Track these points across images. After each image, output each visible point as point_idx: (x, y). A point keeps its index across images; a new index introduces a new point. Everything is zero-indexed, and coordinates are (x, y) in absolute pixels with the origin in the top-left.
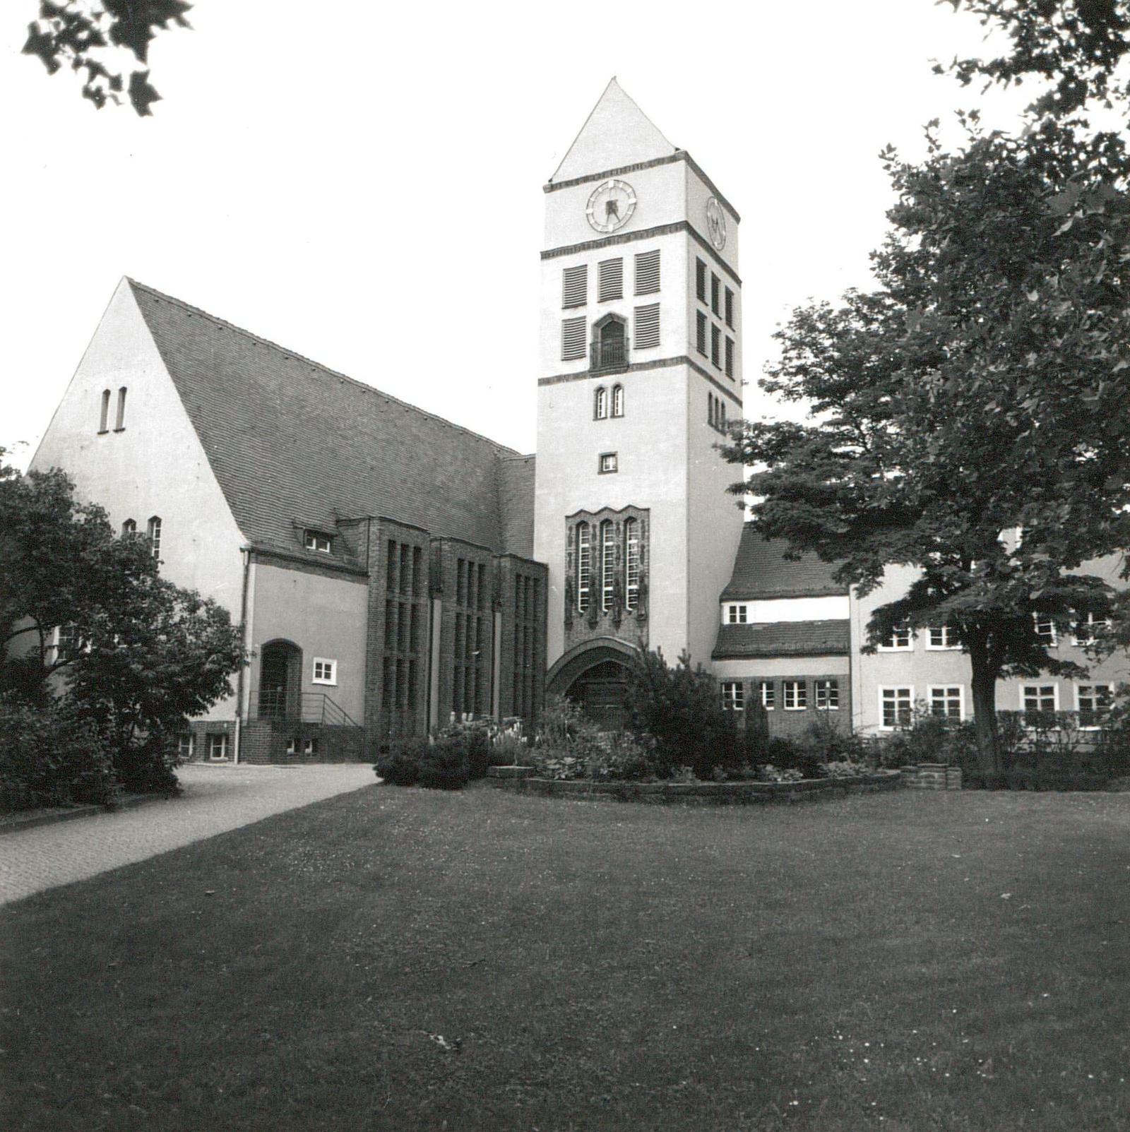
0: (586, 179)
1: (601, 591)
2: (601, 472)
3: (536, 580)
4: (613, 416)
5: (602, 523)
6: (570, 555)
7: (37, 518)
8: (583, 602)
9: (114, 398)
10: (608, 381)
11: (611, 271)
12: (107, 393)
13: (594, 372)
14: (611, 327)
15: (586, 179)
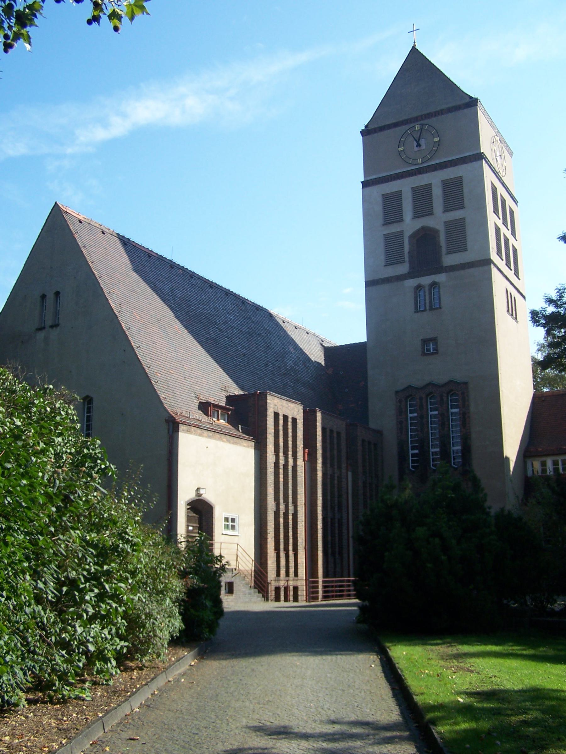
0: (396, 125)
1: (429, 451)
2: (424, 354)
3: (375, 445)
4: (431, 309)
5: (427, 395)
6: (401, 423)
7: (32, 20)
8: (413, 462)
10: (426, 281)
11: (422, 197)
12: (43, 297)
13: (411, 275)
14: (425, 239)
15: (396, 125)
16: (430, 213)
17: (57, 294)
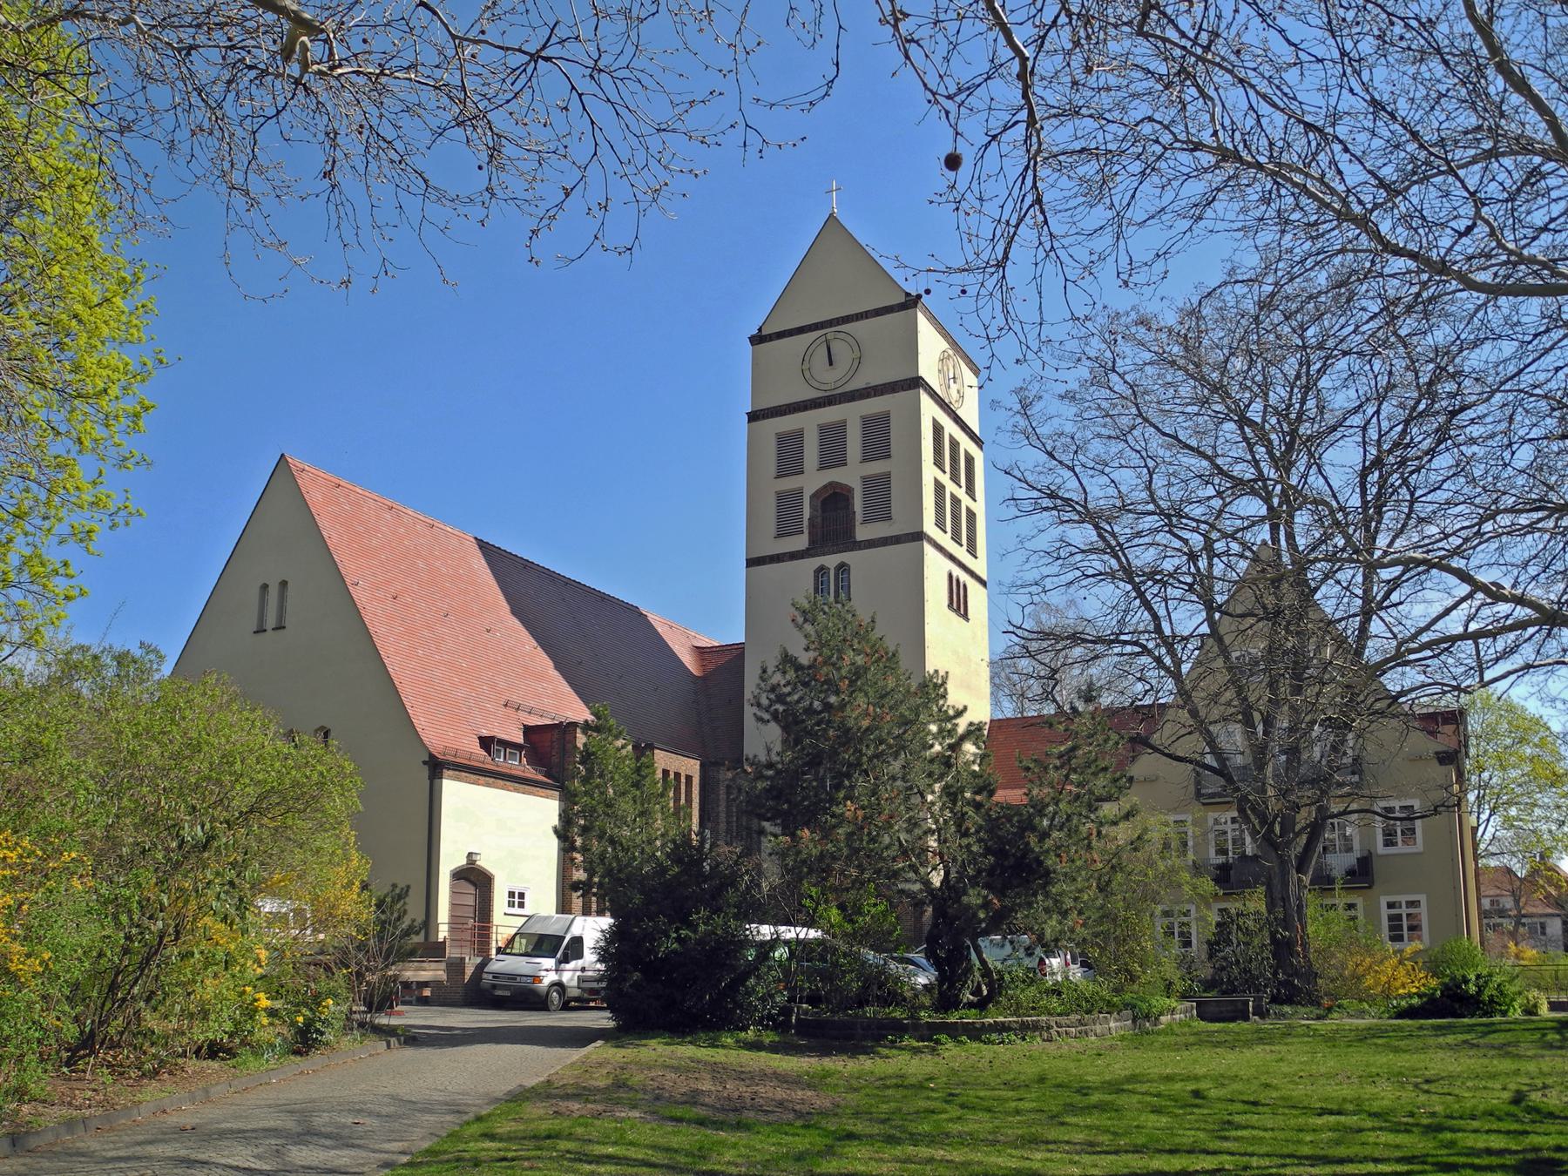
9: (271, 622)
10: (831, 561)
11: (833, 437)
12: (265, 587)
14: (834, 500)
16: (842, 462)
17: (284, 584)
